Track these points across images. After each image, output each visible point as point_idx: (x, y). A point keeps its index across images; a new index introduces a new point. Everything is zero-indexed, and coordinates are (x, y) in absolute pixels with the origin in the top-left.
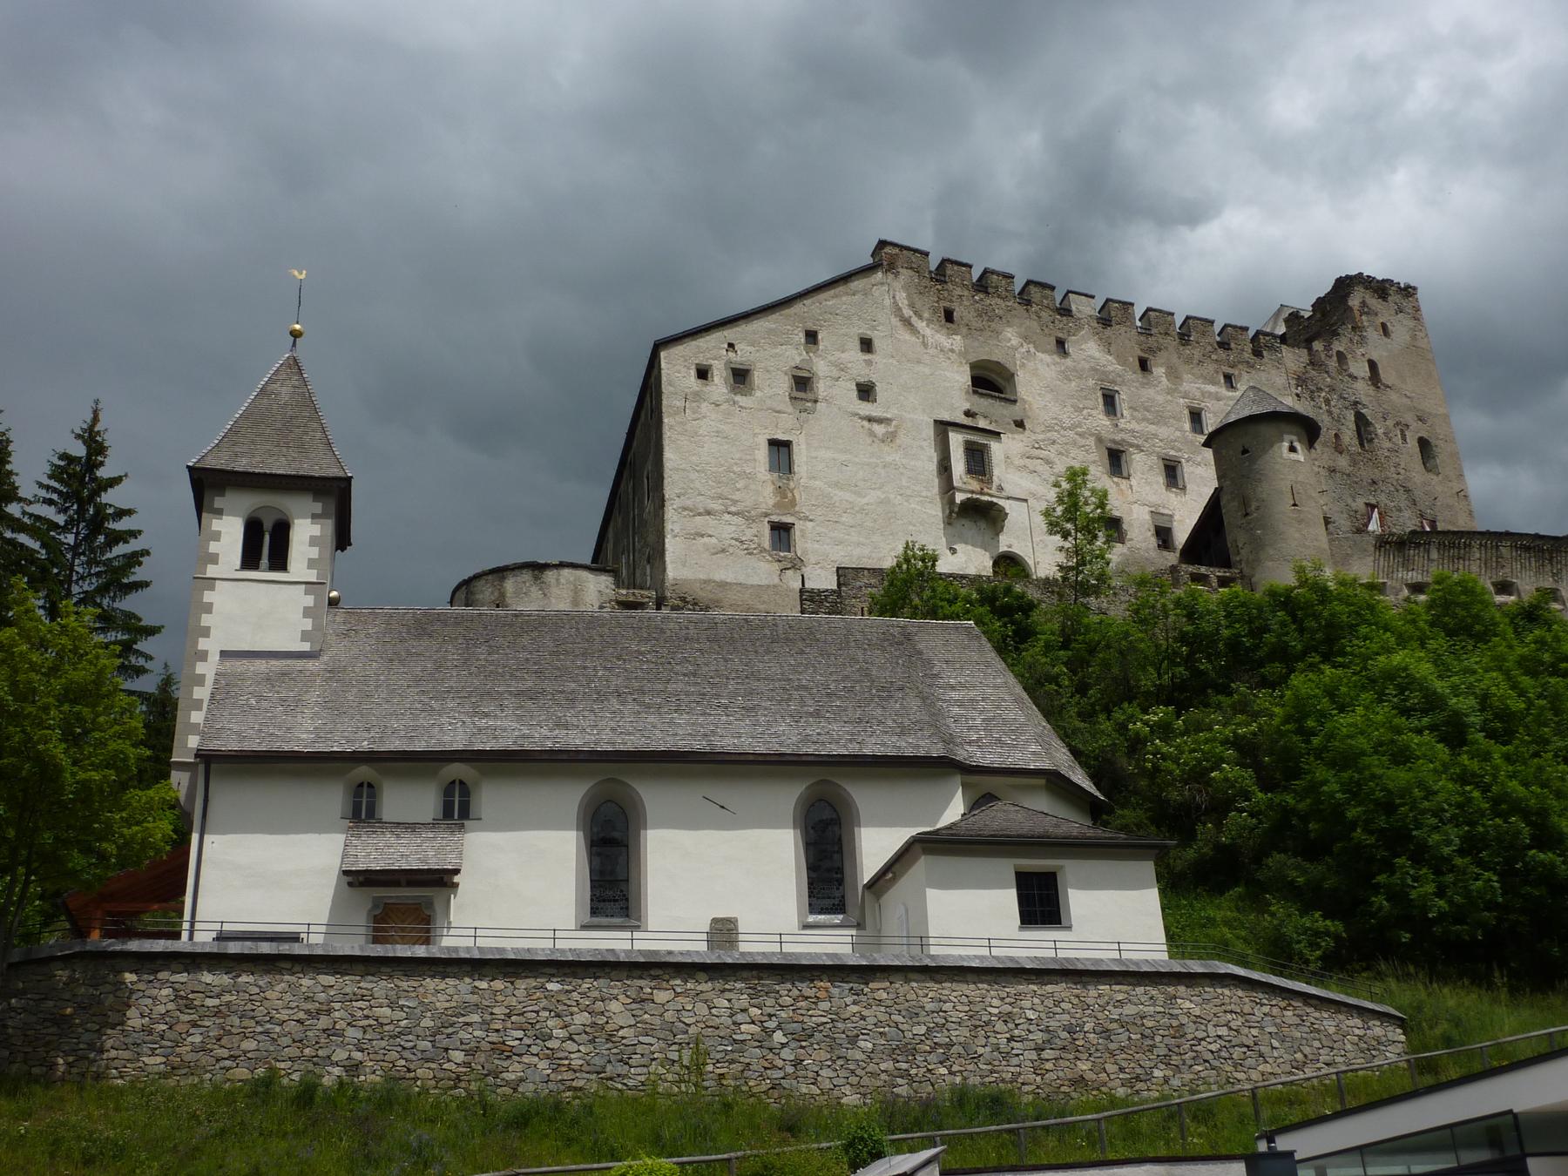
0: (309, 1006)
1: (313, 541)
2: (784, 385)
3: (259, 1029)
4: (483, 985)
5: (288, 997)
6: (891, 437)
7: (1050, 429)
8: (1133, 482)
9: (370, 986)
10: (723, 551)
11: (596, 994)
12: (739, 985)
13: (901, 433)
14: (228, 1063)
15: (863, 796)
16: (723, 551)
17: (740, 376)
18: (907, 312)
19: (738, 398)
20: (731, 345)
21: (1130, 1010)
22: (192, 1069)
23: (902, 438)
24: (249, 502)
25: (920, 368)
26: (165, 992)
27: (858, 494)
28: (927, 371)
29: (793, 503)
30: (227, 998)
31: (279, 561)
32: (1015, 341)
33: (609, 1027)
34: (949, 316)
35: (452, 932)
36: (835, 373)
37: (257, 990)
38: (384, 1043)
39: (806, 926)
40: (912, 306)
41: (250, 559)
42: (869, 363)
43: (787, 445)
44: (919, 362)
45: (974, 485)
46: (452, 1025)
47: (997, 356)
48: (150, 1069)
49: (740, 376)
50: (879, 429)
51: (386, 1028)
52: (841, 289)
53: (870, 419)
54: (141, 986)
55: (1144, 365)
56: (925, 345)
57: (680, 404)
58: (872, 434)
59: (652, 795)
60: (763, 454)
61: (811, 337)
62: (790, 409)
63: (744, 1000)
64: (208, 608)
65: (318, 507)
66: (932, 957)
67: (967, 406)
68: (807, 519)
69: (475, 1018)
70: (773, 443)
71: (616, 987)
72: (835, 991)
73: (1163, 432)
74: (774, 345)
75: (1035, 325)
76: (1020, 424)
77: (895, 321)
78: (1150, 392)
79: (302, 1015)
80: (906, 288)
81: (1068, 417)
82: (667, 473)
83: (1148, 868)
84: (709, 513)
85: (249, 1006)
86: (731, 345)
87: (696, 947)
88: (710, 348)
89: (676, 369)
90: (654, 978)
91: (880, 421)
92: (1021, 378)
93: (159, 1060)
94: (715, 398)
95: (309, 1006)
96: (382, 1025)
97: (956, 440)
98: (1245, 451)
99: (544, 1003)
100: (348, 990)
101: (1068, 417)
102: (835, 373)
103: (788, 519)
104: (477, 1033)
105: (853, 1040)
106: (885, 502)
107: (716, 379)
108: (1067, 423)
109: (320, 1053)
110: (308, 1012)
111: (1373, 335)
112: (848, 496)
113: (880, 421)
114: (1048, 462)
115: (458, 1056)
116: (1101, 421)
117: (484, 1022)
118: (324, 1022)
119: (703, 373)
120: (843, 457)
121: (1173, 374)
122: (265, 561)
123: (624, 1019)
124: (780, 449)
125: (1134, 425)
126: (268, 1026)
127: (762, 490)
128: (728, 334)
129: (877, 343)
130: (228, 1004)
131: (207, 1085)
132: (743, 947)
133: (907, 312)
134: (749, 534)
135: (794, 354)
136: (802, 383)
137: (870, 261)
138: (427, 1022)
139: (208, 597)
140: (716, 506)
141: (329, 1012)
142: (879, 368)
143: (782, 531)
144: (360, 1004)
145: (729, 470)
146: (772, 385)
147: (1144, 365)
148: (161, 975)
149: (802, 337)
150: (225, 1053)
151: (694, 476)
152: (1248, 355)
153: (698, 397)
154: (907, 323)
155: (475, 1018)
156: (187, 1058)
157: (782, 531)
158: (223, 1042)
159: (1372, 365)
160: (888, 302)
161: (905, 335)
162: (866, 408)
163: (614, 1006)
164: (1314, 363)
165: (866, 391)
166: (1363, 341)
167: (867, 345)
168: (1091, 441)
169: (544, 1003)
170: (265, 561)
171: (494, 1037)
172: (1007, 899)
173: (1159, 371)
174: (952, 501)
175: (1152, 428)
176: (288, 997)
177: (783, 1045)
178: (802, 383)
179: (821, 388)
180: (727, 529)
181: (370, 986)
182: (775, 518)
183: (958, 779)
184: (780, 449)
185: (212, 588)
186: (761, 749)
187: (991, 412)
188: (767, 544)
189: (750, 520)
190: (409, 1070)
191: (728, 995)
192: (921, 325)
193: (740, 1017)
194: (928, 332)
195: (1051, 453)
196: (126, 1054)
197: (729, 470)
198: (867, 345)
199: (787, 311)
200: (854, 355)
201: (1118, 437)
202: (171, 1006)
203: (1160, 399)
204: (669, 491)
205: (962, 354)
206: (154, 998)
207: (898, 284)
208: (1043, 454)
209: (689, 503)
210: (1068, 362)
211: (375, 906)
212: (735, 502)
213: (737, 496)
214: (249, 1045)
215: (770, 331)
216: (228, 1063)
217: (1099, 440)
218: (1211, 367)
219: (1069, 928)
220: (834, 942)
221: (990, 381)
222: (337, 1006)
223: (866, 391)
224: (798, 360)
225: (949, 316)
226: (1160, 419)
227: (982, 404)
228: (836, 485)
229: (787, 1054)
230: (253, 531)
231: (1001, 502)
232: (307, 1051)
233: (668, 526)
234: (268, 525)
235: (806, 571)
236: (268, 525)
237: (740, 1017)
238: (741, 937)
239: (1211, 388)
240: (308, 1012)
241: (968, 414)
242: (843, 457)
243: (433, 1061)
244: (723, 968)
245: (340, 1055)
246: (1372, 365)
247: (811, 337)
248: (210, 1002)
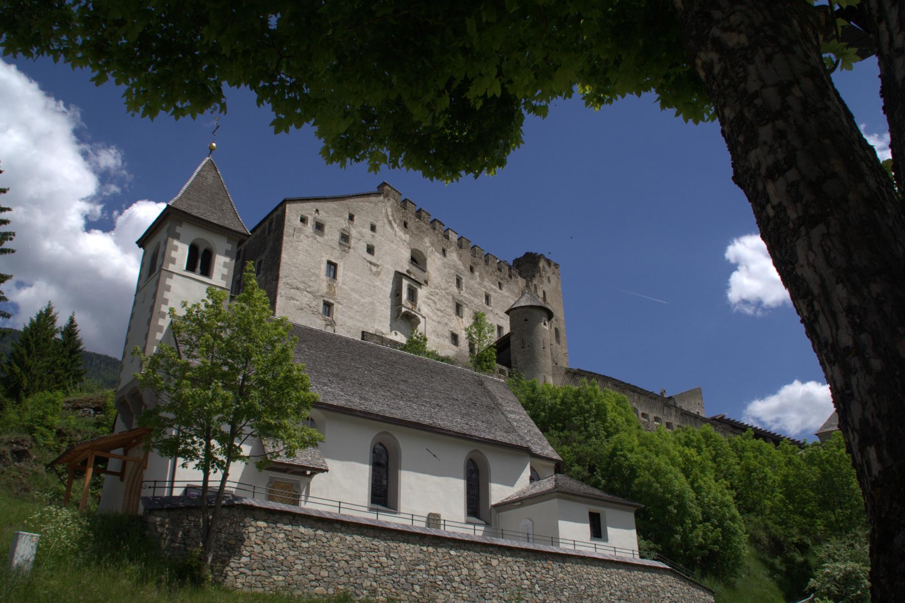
0: (350, 552)
1: (173, 261)
2: (337, 237)
3: (329, 564)
4: (425, 548)
5: (340, 546)
6: (377, 274)
7: (436, 288)
8: (464, 320)
9: (377, 544)
10: (302, 309)
11: (469, 559)
12: (522, 560)
13: (382, 273)
14: (314, 583)
15: (495, 463)
16: (302, 309)
17: (319, 227)
18: (391, 218)
19: (317, 237)
20: (317, 211)
21: (644, 583)
22: (299, 586)
23: (382, 276)
24: (193, 233)
25: (393, 245)
26: (282, 535)
27: (362, 297)
28: (395, 247)
29: (334, 293)
30: (312, 543)
31: (206, 271)
32: (428, 244)
33: (477, 577)
34: (405, 225)
35: (402, 515)
36: (359, 237)
37: (325, 540)
38: (385, 578)
39: (468, 523)
40: (393, 216)
41: (191, 267)
42: (373, 236)
43: (335, 265)
44: (392, 242)
45: (410, 306)
46: (414, 570)
47: (421, 249)
48: (277, 583)
49: (319, 227)
50: (374, 269)
51: (387, 569)
52: (365, 199)
53: (371, 263)
54: (269, 530)
55: (472, 270)
56: (395, 235)
57: (292, 232)
58: (371, 270)
59: (408, 447)
60: (324, 266)
61: (351, 217)
62: (338, 248)
63: (523, 568)
64: (168, 288)
65: (229, 247)
66: (303, 509)
67: (408, 268)
68: (339, 303)
69: (422, 567)
70: (330, 263)
71: (477, 556)
72: (554, 566)
73: (476, 301)
74: (336, 216)
75: (436, 239)
76: (426, 282)
77: (386, 220)
78: (472, 282)
79: (347, 558)
80: (391, 206)
81: (443, 285)
82: (282, 264)
83: (630, 517)
84: (298, 289)
85: (323, 550)
86: (317, 211)
87: (420, 525)
88: (307, 209)
89: (292, 213)
90: (491, 553)
91: (375, 265)
92: (429, 261)
93: (281, 578)
94: (307, 233)
95: (350, 552)
96: (384, 567)
97: (405, 283)
98: (526, 320)
99: (450, 562)
100: (368, 545)
101: (443, 285)
102: (359, 237)
103: (332, 301)
104: (425, 576)
105: (562, 591)
106: (372, 303)
107: (309, 225)
108: (443, 287)
109: (358, 581)
110: (350, 556)
111: (545, 280)
112: (357, 296)
113: (375, 265)
114: (435, 303)
115: (417, 588)
116: (455, 289)
117: (426, 570)
118: (357, 563)
119: (303, 220)
120: (357, 278)
121: (481, 277)
122: (198, 269)
123: (481, 573)
124: (332, 266)
125: (466, 295)
126: (332, 563)
127: (322, 283)
128: (318, 205)
129: (377, 228)
130: (313, 547)
131: (305, 596)
132: (561, 545)
133: (391, 218)
134: (314, 304)
135: (343, 223)
136: (345, 238)
137: (376, 190)
138: (403, 568)
139: (169, 282)
140: (301, 286)
141: (360, 557)
142: (377, 240)
143: (328, 306)
144: (373, 554)
145: (309, 270)
146: (332, 235)
147: (472, 270)
148: (278, 525)
149: (347, 216)
150: (312, 577)
151: (293, 269)
152: (507, 276)
153: (300, 231)
154: (390, 222)
155: (422, 567)
156: (295, 578)
157: (328, 306)
158: (312, 570)
159: (544, 293)
160: (384, 211)
161: (388, 228)
162: (369, 257)
163: (477, 566)
164: (527, 286)
165: (370, 250)
166: (542, 282)
167: (373, 228)
168: (450, 298)
169: (450, 562)
170: (198, 269)
171: (431, 579)
172: (586, 528)
173: (477, 274)
174: (400, 310)
175: (472, 298)
176: (340, 546)
177: (539, 592)
178: (345, 238)
179: (353, 242)
180: (305, 299)
181: (377, 544)
182: (326, 299)
183: (528, 458)
184: (332, 266)
185: (171, 278)
186: (456, 429)
187: (417, 274)
188: (321, 311)
189: (315, 297)
190: (397, 595)
191: (518, 564)
192: (395, 226)
193: (523, 576)
194: (397, 230)
195: (436, 298)
196: (264, 573)
197: (309, 270)
198: (373, 228)
199: (342, 202)
200: (367, 231)
201: (460, 298)
202: (285, 545)
203: (476, 286)
204: (282, 273)
205: (409, 244)
206: (276, 539)
207: (389, 204)
208: (433, 298)
209: (289, 281)
210: (446, 260)
211: (270, 482)
212: (310, 287)
213: (311, 284)
214: (324, 573)
215: (335, 209)
216: (314, 583)
217: (454, 298)
218: (495, 278)
219: (606, 540)
220: (476, 532)
221: (417, 260)
222: (364, 554)
223: (370, 250)
224: (344, 226)
225: (405, 225)
226: (475, 295)
227: (414, 269)
228: (353, 290)
229: (540, 596)
230: (193, 250)
231: (419, 317)
232: (352, 579)
233: (279, 291)
234: (201, 250)
235: (337, 328)
236: (201, 250)
237: (523, 576)
238: (425, 519)
239: (494, 287)
240: (350, 556)
241: (408, 271)
242: (357, 278)
243: (407, 590)
244: (431, 538)
245: (367, 583)
246: (544, 293)
247: (351, 217)
248: (305, 545)
